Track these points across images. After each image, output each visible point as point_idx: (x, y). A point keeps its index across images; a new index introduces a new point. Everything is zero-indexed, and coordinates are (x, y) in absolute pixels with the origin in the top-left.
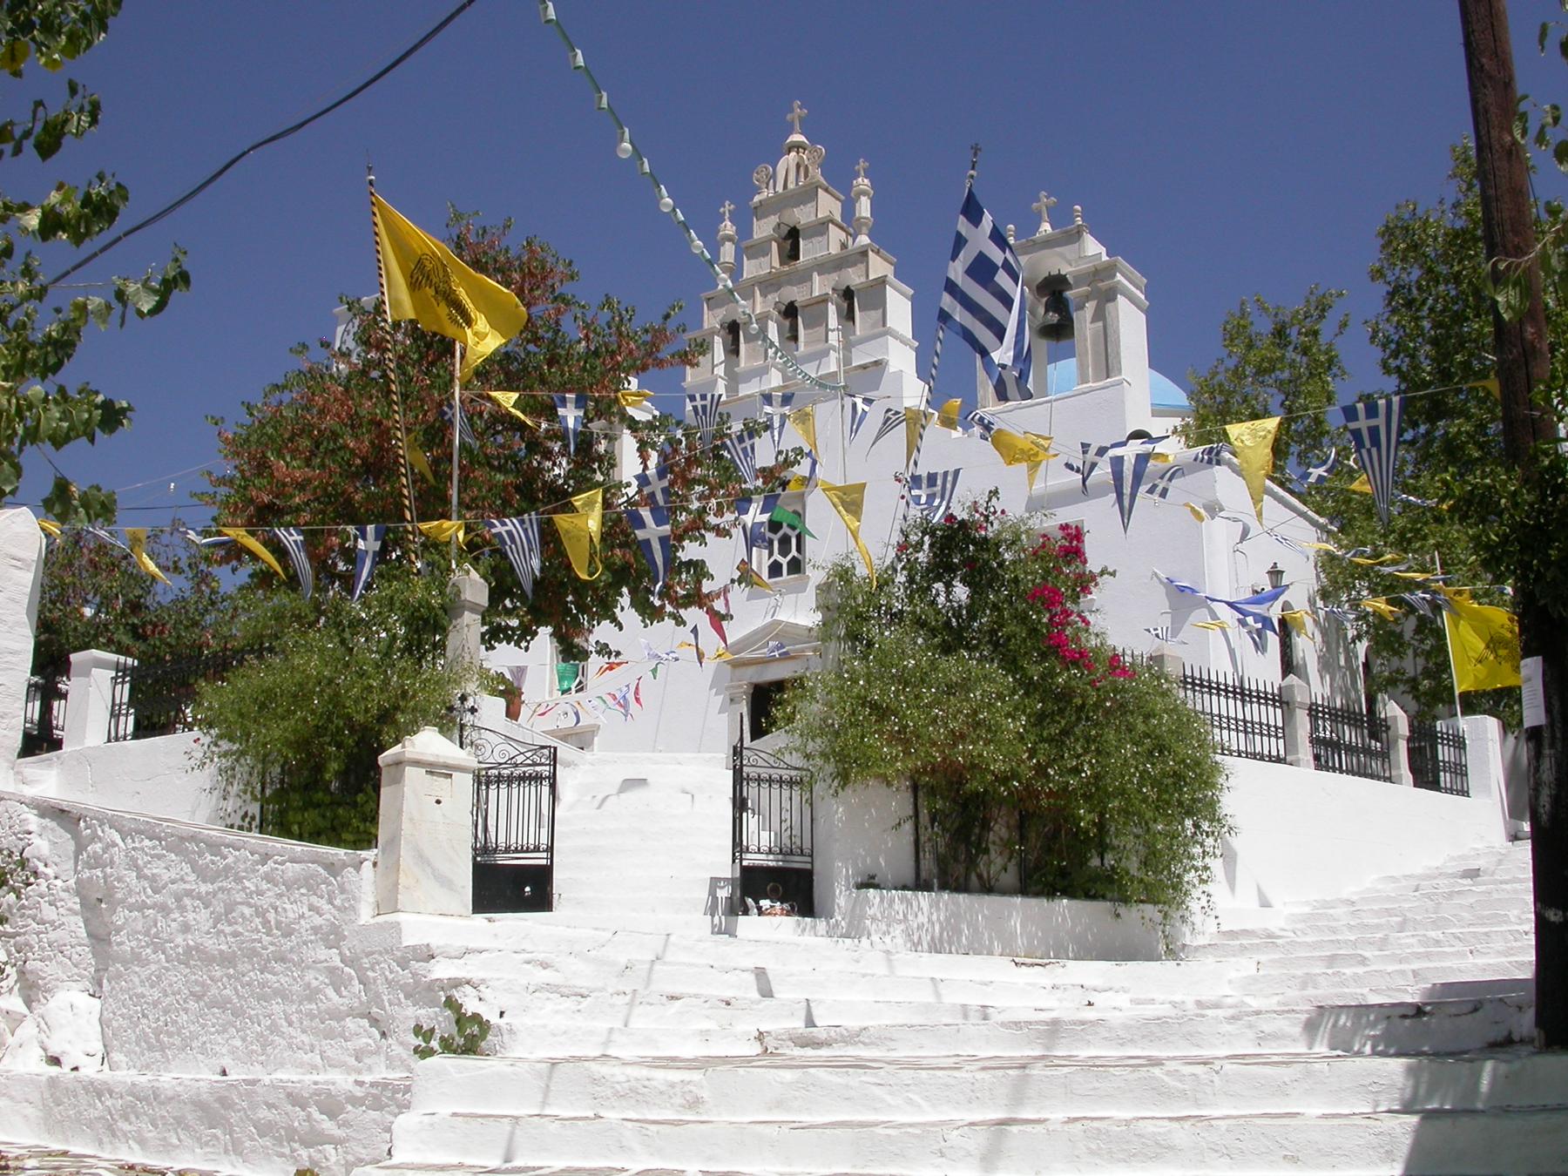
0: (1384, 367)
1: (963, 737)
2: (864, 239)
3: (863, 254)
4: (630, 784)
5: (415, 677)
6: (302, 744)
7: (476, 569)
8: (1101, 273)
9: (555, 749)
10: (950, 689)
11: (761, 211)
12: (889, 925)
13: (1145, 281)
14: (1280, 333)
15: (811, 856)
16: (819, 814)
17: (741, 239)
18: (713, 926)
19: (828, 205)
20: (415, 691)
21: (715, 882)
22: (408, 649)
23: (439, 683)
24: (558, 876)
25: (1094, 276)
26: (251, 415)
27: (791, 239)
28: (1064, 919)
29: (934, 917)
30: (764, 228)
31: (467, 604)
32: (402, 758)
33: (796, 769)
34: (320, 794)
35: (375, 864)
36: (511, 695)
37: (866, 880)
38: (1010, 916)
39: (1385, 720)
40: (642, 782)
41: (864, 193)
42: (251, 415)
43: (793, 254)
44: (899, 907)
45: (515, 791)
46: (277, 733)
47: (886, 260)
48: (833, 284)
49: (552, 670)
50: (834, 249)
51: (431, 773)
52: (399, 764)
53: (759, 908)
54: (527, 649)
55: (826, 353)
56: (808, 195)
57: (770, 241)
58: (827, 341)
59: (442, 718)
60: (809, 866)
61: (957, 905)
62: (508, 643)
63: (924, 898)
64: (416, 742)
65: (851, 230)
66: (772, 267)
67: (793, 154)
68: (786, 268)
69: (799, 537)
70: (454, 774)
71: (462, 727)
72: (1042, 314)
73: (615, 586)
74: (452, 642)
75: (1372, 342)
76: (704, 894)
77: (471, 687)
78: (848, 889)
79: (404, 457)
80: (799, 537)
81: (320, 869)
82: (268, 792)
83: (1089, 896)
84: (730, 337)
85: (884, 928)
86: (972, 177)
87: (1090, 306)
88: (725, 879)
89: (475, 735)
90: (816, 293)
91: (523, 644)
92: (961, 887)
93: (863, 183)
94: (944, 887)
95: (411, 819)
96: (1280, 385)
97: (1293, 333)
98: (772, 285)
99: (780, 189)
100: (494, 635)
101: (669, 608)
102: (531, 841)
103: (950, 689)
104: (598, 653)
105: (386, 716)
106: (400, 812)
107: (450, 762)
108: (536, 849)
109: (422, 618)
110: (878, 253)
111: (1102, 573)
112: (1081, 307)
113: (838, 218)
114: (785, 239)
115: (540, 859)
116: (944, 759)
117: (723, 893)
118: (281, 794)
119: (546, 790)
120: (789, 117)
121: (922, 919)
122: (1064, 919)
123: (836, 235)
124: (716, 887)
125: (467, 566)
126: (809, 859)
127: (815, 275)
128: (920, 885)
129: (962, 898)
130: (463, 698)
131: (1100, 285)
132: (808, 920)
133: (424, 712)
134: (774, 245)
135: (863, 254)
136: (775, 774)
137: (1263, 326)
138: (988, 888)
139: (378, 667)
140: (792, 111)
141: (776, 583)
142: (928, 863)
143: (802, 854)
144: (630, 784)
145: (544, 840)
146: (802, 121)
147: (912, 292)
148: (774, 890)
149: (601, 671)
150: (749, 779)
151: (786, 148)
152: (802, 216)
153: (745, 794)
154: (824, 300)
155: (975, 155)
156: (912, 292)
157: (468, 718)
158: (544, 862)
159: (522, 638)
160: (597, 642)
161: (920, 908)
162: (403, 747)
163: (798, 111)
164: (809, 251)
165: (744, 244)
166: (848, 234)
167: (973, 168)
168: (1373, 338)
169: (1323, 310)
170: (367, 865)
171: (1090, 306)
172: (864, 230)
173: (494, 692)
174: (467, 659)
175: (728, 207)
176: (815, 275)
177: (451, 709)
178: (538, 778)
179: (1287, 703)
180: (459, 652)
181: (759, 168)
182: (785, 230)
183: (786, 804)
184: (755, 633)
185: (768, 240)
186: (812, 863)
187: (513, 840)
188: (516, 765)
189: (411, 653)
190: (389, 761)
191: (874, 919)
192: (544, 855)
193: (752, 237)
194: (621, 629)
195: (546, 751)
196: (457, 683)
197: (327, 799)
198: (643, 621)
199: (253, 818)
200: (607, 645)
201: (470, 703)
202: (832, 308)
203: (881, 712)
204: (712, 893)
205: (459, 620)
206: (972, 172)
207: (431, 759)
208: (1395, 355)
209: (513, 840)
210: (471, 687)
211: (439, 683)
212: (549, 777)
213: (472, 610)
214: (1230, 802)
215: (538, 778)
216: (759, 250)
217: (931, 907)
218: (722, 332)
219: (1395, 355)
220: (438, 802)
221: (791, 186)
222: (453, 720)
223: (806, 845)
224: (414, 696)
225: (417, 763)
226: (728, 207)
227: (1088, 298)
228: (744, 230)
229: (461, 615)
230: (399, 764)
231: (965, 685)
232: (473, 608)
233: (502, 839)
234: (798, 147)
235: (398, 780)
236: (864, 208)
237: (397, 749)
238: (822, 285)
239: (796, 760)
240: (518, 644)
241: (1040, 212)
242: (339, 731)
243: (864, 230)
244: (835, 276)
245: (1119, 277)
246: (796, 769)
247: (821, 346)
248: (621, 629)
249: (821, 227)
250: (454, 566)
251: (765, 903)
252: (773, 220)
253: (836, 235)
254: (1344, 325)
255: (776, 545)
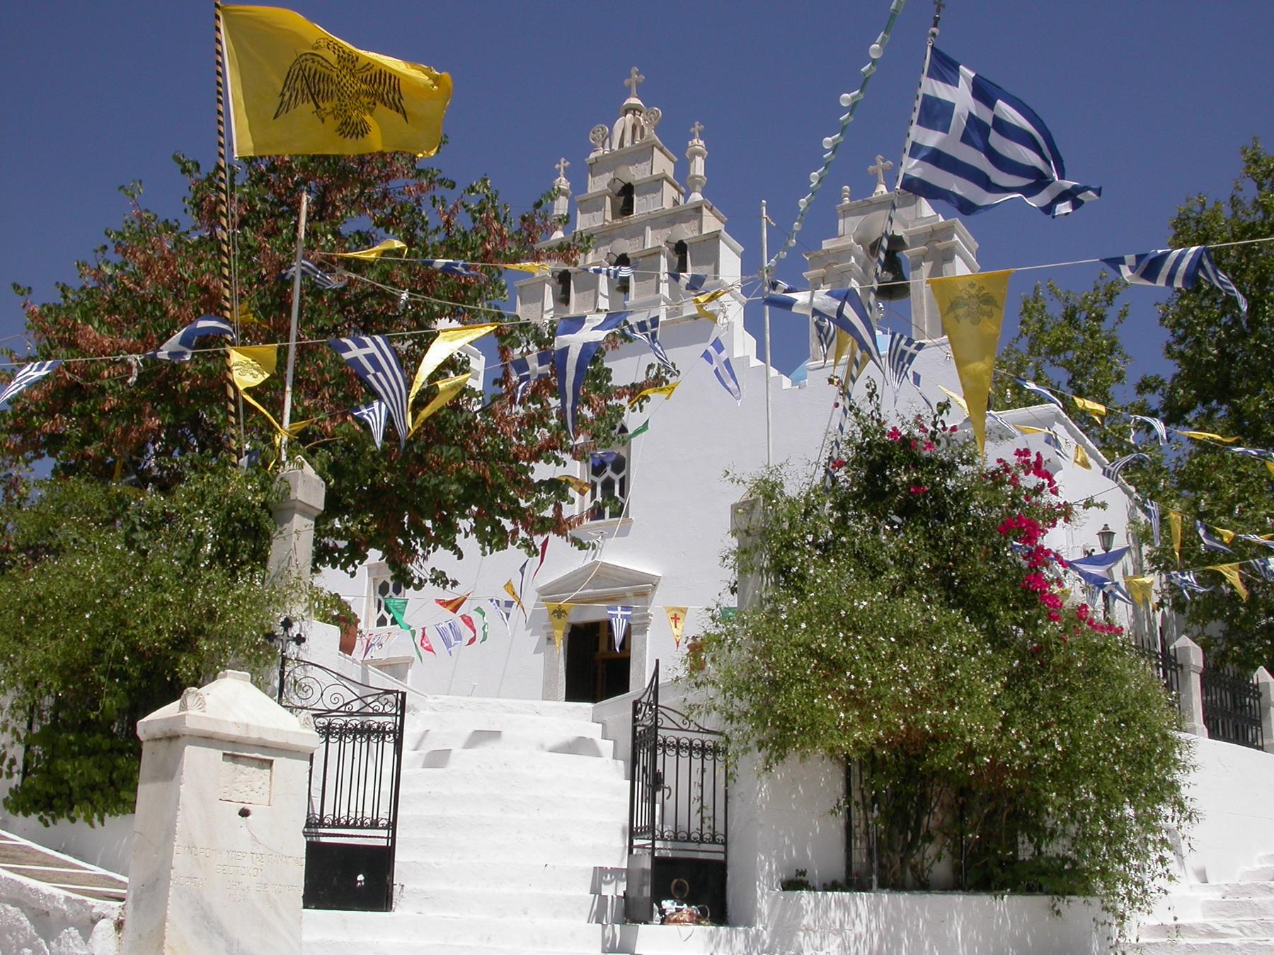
0: (1169, 352)
1: (927, 702)
2: (697, 197)
3: (698, 210)
4: (481, 737)
5: (226, 594)
6: (73, 672)
7: (311, 464)
8: (935, 235)
9: (404, 694)
10: (906, 639)
11: (596, 168)
12: (823, 938)
13: (977, 246)
14: (1070, 317)
15: (725, 843)
16: (735, 790)
17: (575, 194)
18: (604, 941)
19: (662, 164)
20: (225, 612)
21: (600, 875)
22: (218, 557)
23: (258, 602)
24: (400, 857)
25: (931, 236)
26: (65, 297)
27: (625, 195)
28: (1005, 921)
29: (873, 925)
30: (598, 184)
31: (298, 505)
32: (180, 729)
33: (709, 732)
34: (98, 737)
35: (119, 925)
36: (345, 620)
37: (793, 875)
38: (952, 918)
39: (1257, 686)
40: (496, 735)
41: (700, 153)
42: (65, 297)
43: (627, 209)
44: (835, 914)
45: (349, 747)
46: (39, 655)
47: (717, 217)
48: (665, 238)
49: (369, 602)
50: (668, 205)
51: (234, 758)
52: (173, 738)
53: (662, 912)
54: (353, 574)
55: (657, 303)
56: (643, 154)
57: (604, 196)
58: (658, 291)
59: (257, 648)
60: (721, 857)
61: (896, 907)
62: (334, 567)
63: (862, 901)
64: (207, 699)
65: (683, 190)
66: (605, 221)
67: (629, 116)
68: (619, 222)
69: (622, 482)
70: (279, 762)
71: (284, 660)
72: (878, 274)
73: (465, 502)
74: (276, 552)
75: (1161, 324)
76: (583, 891)
77: (297, 610)
78: (771, 889)
79: (228, 266)
80: (622, 482)
81: (23, 918)
82: (36, 729)
83: (1030, 890)
84: (560, 287)
85: (818, 941)
86: (934, 35)
87: (926, 267)
88: (616, 872)
89: (299, 672)
90: (649, 246)
91: (351, 569)
92: (897, 886)
93: (698, 144)
94: (883, 885)
95: (191, 847)
96: (1068, 365)
97: (1081, 316)
98: (604, 237)
99: (615, 147)
100: (322, 555)
101: (522, 534)
102: (368, 813)
103: (906, 639)
104: (433, 581)
105: (184, 642)
106: (170, 832)
107: (271, 738)
108: (374, 825)
109: (239, 520)
110: (711, 210)
111: (1088, 504)
112: (917, 266)
113: (670, 174)
114: (619, 195)
115: (378, 838)
116: (909, 729)
117: (614, 890)
118: (47, 737)
119: (389, 747)
120: (626, 82)
121: (860, 928)
122: (1005, 921)
123: (669, 192)
124: (601, 882)
125: (300, 458)
126: (721, 848)
127: (648, 228)
128: (852, 882)
129: (903, 899)
130: (287, 624)
131: (938, 244)
132: (723, 930)
133: (236, 639)
134: (608, 200)
135: (698, 210)
136: (684, 737)
137: (1056, 311)
138: (923, 885)
139: (179, 577)
140: (630, 76)
141: (598, 525)
142: (859, 857)
143: (714, 841)
144: (481, 737)
145: (384, 812)
146: (638, 86)
147: (742, 249)
148: (680, 888)
149: (1055, 492)
150: (665, 745)
151: (622, 110)
152: (636, 173)
153: (659, 767)
154: (656, 253)
155: (938, 11)
156: (742, 249)
157: (292, 648)
158: (383, 843)
159: (350, 561)
160: (433, 569)
161: (858, 915)
162: (184, 707)
163: (636, 77)
164: (641, 206)
165: (578, 198)
166: (680, 192)
167: (935, 26)
168: (1162, 320)
169: (1111, 297)
170: (105, 926)
171: (926, 267)
172: (698, 188)
173: (325, 618)
174: (295, 574)
175: (563, 164)
176: (648, 228)
177: (271, 636)
178: (381, 732)
179: (1182, 666)
180: (285, 564)
181: (596, 128)
182: (619, 186)
183: (696, 777)
184: (575, 573)
185: (602, 196)
186: (725, 853)
187: (344, 812)
188: (351, 714)
189: (223, 564)
190: (156, 731)
191: (807, 930)
192: (384, 833)
193: (586, 191)
194: (460, 557)
195: (391, 697)
196: (279, 602)
197: (106, 744)
198: (483, 549)
199: (13, 762)
200: (443, 574)
201: (294, 631)
202: (664, 261)
203: (834, 666)
204: (595, 890)
205: (286, 526)
206: (934, 30)
207: (234, 732)
208: (1181, 340)
209: (344, 812)
210: (297, 610)
211: (258, 602)
212: (394, 732)
213: (304, 513)
214: (1193, 786)
215: (381, 732)
216: (593, 205)
217: (869, 912)
218: (553, 282)
219: (1181, 340)
220: (244, 813)
221: (627, 144)
222: (272, 652)
223: (720, 828)
224: (222, 618)
225: (207, 739)
226: (563, 164)
227: (924, 257)
228: (579, 185)
229: (289, 520)
230: (173, 738)
231: (931, 634)
232: (305, 511)
233: (328, 811)
234: (634, 109)
235: (169, 772)
236: (698, 167)
237: (169, 711)
238: (655, 238)
239: (712, 721)
240: (344, 567)
241: (876, 175)
242: (118, 658)
243: (698, 188)
244: (668, 231)
245: (956, 238)
246: (709, 732)
247: (652, 297)
248: (460, 557)
249: (655, 184)
250: (284, 458)
251: (668, 905)
252: (608, 176)
253: (669, 192)
254: (1124, 314)
255: (599, 489)
